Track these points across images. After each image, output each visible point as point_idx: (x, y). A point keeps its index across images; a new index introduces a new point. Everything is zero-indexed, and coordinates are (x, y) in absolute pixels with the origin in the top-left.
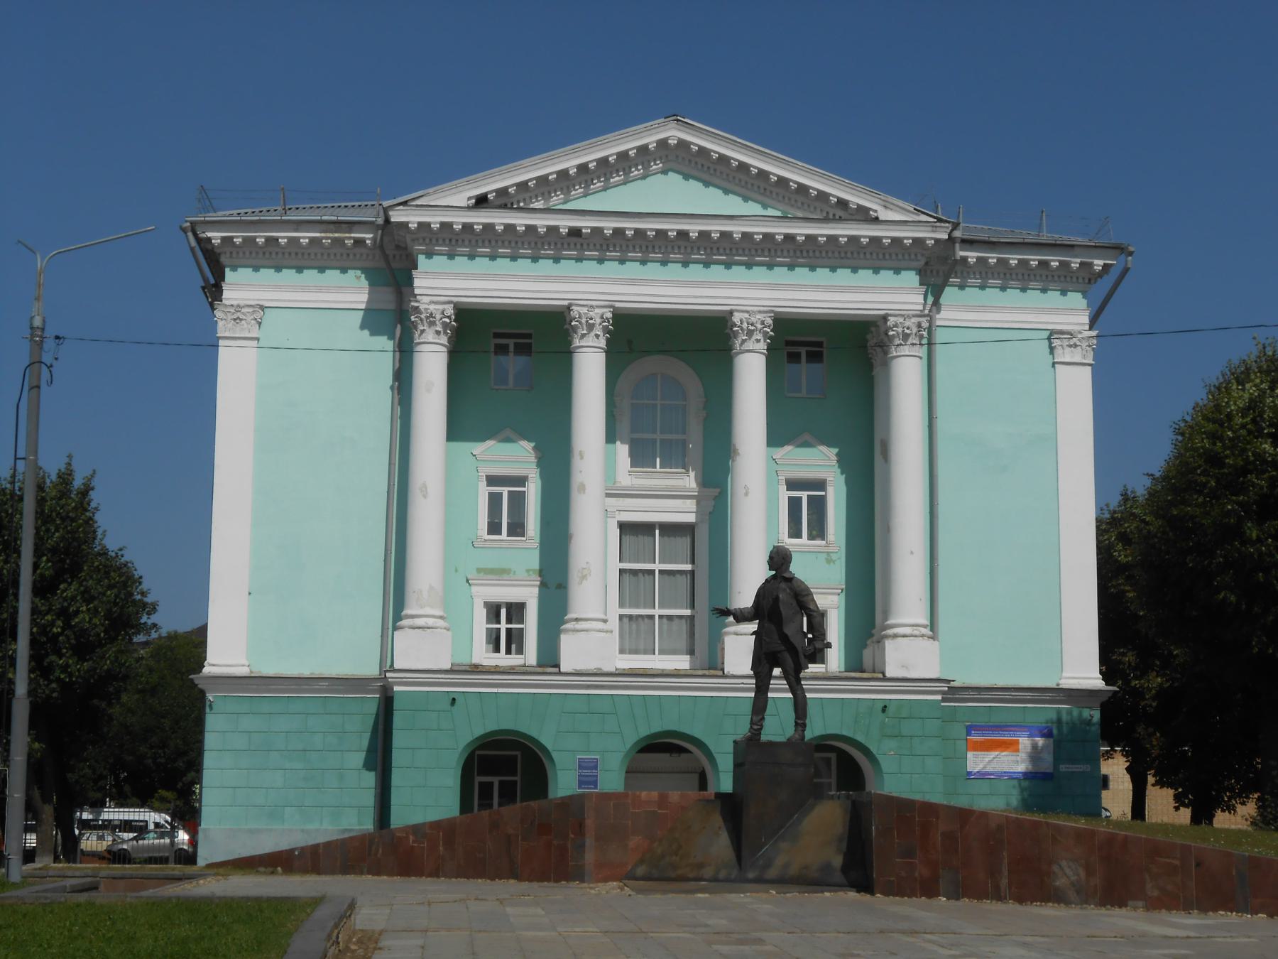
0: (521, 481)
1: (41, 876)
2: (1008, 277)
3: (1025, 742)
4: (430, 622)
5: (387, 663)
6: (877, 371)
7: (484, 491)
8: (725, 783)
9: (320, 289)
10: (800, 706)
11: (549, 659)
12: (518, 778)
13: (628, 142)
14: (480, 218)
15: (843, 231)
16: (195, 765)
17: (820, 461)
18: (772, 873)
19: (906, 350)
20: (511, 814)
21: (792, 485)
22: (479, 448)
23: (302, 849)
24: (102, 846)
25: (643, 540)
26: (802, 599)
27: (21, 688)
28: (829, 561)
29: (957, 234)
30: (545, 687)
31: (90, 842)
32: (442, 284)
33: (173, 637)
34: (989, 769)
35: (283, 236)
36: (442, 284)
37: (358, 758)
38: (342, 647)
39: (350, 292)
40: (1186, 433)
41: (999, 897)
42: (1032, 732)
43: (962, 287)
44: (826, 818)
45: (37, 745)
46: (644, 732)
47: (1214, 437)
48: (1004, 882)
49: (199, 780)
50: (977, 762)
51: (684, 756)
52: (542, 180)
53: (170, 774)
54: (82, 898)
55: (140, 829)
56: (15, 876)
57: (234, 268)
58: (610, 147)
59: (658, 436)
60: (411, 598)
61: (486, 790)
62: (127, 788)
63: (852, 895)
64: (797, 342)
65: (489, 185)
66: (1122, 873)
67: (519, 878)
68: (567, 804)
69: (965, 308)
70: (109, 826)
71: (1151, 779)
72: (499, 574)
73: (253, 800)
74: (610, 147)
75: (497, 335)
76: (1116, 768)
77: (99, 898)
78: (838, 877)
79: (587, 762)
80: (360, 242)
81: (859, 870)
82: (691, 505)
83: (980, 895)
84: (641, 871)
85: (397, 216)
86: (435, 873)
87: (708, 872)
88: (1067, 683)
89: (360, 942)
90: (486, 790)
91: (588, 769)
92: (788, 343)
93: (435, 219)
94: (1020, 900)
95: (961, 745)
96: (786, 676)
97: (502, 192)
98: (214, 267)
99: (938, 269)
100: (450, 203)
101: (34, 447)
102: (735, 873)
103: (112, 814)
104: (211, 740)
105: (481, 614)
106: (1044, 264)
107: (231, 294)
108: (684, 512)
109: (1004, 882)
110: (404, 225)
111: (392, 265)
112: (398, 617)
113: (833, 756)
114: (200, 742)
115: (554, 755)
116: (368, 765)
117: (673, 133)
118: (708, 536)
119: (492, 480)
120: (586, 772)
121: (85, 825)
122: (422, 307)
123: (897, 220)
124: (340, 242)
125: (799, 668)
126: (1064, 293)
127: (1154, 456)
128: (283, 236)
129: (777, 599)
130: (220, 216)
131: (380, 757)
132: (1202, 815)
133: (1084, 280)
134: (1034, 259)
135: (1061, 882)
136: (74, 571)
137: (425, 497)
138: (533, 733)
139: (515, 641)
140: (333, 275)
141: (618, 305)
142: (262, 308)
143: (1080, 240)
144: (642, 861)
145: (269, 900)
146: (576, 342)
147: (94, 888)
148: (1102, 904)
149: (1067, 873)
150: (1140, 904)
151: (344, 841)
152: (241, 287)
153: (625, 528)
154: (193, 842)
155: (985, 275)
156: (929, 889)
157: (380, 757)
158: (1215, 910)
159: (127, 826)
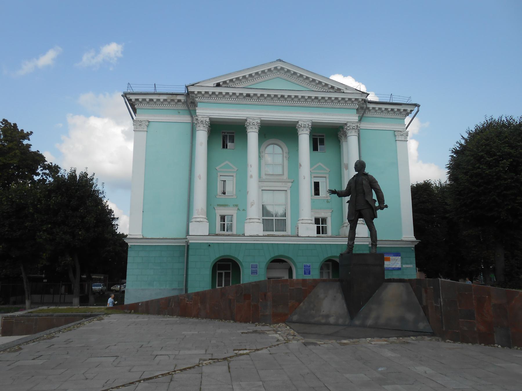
4: (202, 220)
12: (230, 271)
14: (218, 90)
15: (333, 95)
18: (370, 322)
23: (142, 303)
36: (207, 111)
46: (273, 256)
51: (284, 263)
67: (235, 321)
75: (223, 133)
80: (179, 101)
86: (197, 316)
90: (220, 275)
92: (314, 136)
102: (347, 322)
104: (129, 260)
105: (218, 219)
113: (330, 263)
115: (243, 263)
120: (254, 269)
122: (199, 119)
137: (200, 179)
138: (236, 256)
141: (262, 119)
142: (149, 122)
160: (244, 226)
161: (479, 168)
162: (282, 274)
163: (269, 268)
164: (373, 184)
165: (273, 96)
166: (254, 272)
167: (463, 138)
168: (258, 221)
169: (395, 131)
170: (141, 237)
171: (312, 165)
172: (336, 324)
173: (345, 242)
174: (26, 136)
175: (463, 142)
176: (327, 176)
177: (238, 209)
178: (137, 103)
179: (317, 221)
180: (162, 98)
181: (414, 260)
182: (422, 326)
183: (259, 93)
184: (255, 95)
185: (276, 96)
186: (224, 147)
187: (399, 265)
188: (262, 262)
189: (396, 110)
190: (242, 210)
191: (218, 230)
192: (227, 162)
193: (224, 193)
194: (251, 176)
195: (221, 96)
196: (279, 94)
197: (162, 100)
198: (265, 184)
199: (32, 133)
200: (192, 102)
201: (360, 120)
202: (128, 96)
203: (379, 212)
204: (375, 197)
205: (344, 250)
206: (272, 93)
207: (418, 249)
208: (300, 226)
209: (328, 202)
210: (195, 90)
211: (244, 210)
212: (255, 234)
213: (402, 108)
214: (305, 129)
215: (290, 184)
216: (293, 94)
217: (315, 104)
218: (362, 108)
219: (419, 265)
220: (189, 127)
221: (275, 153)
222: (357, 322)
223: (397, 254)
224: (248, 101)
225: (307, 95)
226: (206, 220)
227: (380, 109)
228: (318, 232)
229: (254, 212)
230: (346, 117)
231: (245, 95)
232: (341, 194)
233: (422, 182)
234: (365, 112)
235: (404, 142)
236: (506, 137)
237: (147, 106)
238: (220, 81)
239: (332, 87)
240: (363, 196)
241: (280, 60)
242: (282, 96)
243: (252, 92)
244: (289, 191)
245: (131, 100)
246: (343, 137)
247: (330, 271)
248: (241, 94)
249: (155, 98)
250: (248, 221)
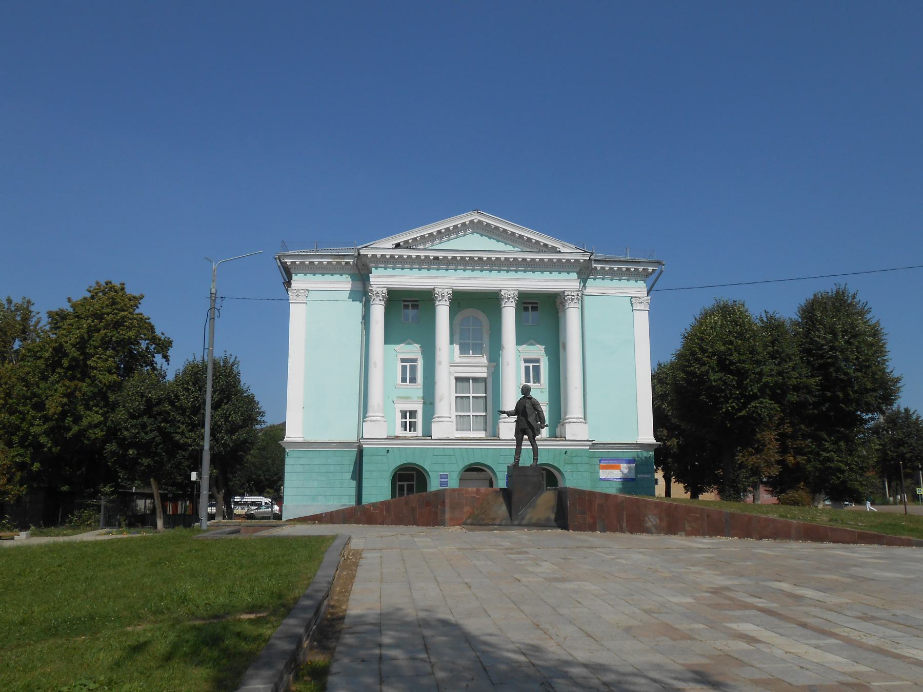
0: (415, 360)
1: (217, 526)
2: (613, 274)
3: (624, 467)
4: (378, 418)
5: (360, 437)
6: (561, 314)
7: (399, 365)
8: (502, 483)
9: (332, 282)
10: (535, 451)
11: (427, 434)
13: (458, 221)
14: (397, 253)
15: (546, 256)
16: (281, 479)
17: (538, 351)
18: (525, 522)
19: (572, 305)
20: (414, 497)
21: (526, 361)
22: (397, 347)
23: (326, 513)
24: (244, 512)
25: (466, 384)
26: (535, 406)
27: (207, 447)
28: (542, 392)
29: (592, 257)
30: (426, 445)
31: (238, 511)
32: (382, 280)
33: (272, 427)
35: (316, 261)
36: (382, 280)
37: (349, 475)
38: (344, 431)
39: (344, 283)
40: (689, 339)
41: (622, 531)
42: (629, 462)
43: (595, 279)
44: (547, 498)
46: (467, 463)
47: (702, 339)
49: (282, 485)
50: (603, 474)
52: (423, 237)
53: (271, 483)
54: (233, 536)
55: (259, 505)
56: (204, 527)
57: (296, 274)
58: (450, 223)
59: (471, 342)
60: (370, 409)
61: (401, 487)
62: (254, 488)
63: (560, 530)
64: (529, 303)
65: (401, 239)
66: (673, 521)
67: (418, 525)
68: (437, 493)
69: (595, 286)
70: (246, 503)
71: (673, 480)
72: (406, 399)
73: (306, 493)
74: (450, 223)
75: (404, 301)
76: (659, 475)
77: (240, 537)
78: (554, 524)
79: (443, 476)
80: (347, 263)
81: (562, 520)
82: (485, 369)
83: (614, 530)
84: (469, 521)
85: (362, 252)
86: (382, 523)
87: (498, 522)
88: (639, 441)
89: (353, 555)
90: (401, 487)
91: (444, 479)
93: (379, 253)
94: (631, 532)
95: (597, 467)
96: (529, 440)
97: (406, 242)
98: (288, 273)
99: (585, 272)
100: (385, 246)
101: (212, 344)
102: (509, 522)
103: (248, 499)
104: (287, 468)
105: (399, 415)
106: (628, 269)
107: (294, 285)
108: (482, 373)
109: (625, 525)
111: (361, 272)
112: (365, 417)
113: (544, 472)
114: (283, 469)
116: (353, 478)
117: (476, 217)
118: (492, 383)
119: (403, 360)
121: (237, 503)
123: (568, 252)
124: (340, 263)
125: (535, 435)
126: (636, 281)
127: (674, 346)
128: (316, 261)
129: (525, 407)
130: (291, 253)
131: (358, 474)
132: (694, 496)
133: (645, 276)
134: (624, 267)
135: (649, 524)
136: (229, 399)
139: (413, 426)
140: (337, 277)
143: (642, 260)
144: (469, 517)
145: (313, 537)
146: (437, 303)
147: (238, 531)
148: (666, 534)
149: (651, 520)
151: (343, 510)
152: (298, 282)
153: (458, 379)
154: (281, 510)
155: (604, 274)
156: (592, 528)
157: (358, 474)
158: (716, 535)
159: (253, 504)
199: (142, 297)
222: (516, 523)
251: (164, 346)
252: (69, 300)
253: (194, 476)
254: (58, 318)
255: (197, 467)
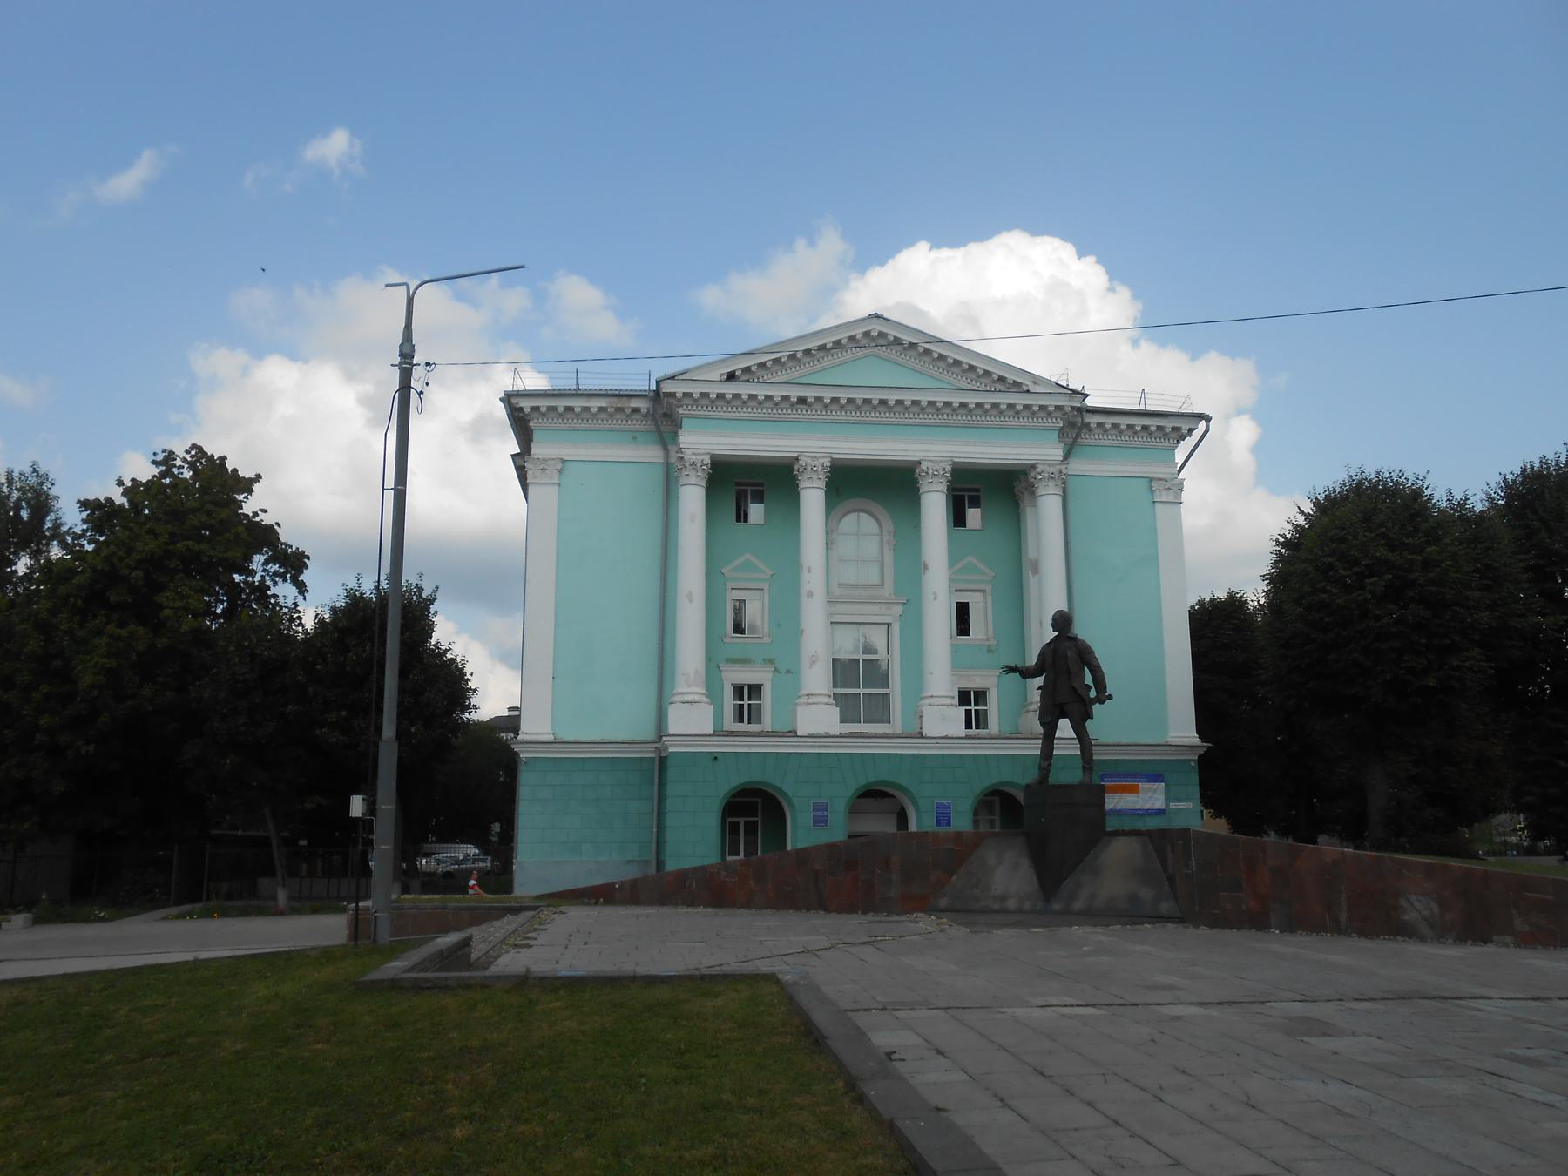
4: (696, 698)
12: (759, 819)
14: (730, 389)
15: (1004, 400)
18: (1078, 905)
23: (622, 883)
34: (1119, 807)
36: (704, 440)
38: (614, 719)
45: (282, 897)
48: (1343, 916)
67: (827, 910)
75: (738, 484)
80: (636, 411)
86: (747, 905)
90: (734, 828)
105: (729, 693)
109: (1343, 916)
110: (672, 395)
113: (997, 799)
142: (564, 461)
150: (1508, 939)
160: (795, 712)
161: (1324, 591)
162: (879, 825)
163: (854, 810)
164: (1085, 656)
165: (860, 402)
166: (820, 821)
167: (1301, 511)
168: (827, 700)
169: (1151, 480)
170: (550, 738)
171: (952, 561)
172: (1020, 911)
173: (1034, 748)
174: (247, 486)
175: (1301, 520)
176: (988, 588)
177: (776, 670)
178: (535, 415)
179: (964, 698)
180: (595, 404)
181: (1195, 790)
182: (1165, 907)
183: (827, 395)
184: (819, 399)
185: (867, 401)
186: (738, 520)
187: (1159, 803)
188: (839, 797)
189: (1153, 429)
190: (791, 673)
191: (729, 723)
192: (748, 556)
193: (738, 628)
194: (810, 594)
195: (737, 403)
196: (876, 396)
197: (594, 410)
198: (841, 608)
199: (259, 477)
200: (665, 415)
201: (1067, 457)
202: (514, 401)
203: (1096, 708)
204: (1089, 680)
205: (1031, 776)
206: (859, 396)
207: (1207, 765)
208: (926, 711)
209: (989, 651)
210: (678, 389)
211: (788, 672)
212: (821, 731)
213: (1168, 424)
214: (936, 480)
215: (900, 608)
216: (908, 397)
217: (962, 419)
218: (1072, 425)
219: (1211, 799)
220: (659, 472)
221: (865, 531)
222: (1056, 906)
223: (1156, 778)
224: (802, 414)
225: (940, 398)
226: (704, 699)
227: (1115, 426)
228: (968, 725)
229: (817, 679)
230: (1034, 451)
231: (794, 400)
232: (1026, 673)
233: (1222, 594)
234: (1078, 435)
235: (1174, 507)
236: (1382, 525)
237: (560, 424)
238: (737, 366)
239: (1002, 379)
240: (1068, 675)
241: (877, 316)
242: (883, 402)
243: (810, 394)
244: (896, 627)
245: (521, 409)
246: (1026, 495)
247: (997, 818)
248: (785, 398)
249: (578, 404)
250: (803, 700)
251: (293, 564)
252: (120, 483)
253: (357, 806)
254: (99, 512)
255: (364, 781)
